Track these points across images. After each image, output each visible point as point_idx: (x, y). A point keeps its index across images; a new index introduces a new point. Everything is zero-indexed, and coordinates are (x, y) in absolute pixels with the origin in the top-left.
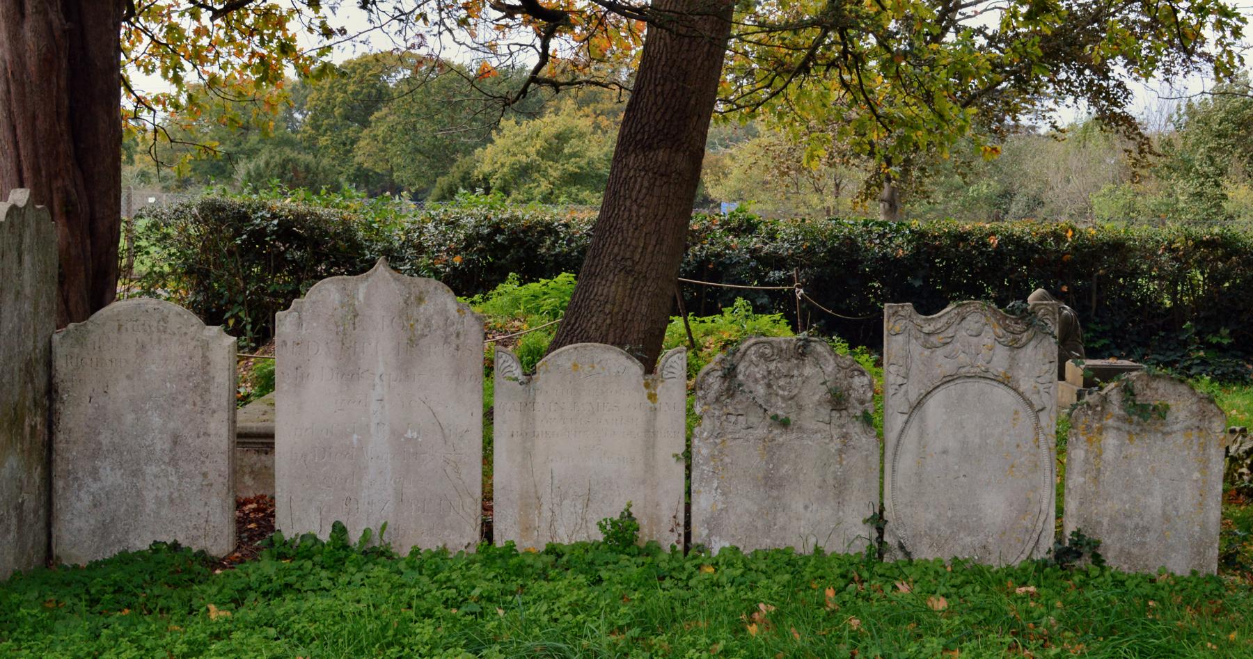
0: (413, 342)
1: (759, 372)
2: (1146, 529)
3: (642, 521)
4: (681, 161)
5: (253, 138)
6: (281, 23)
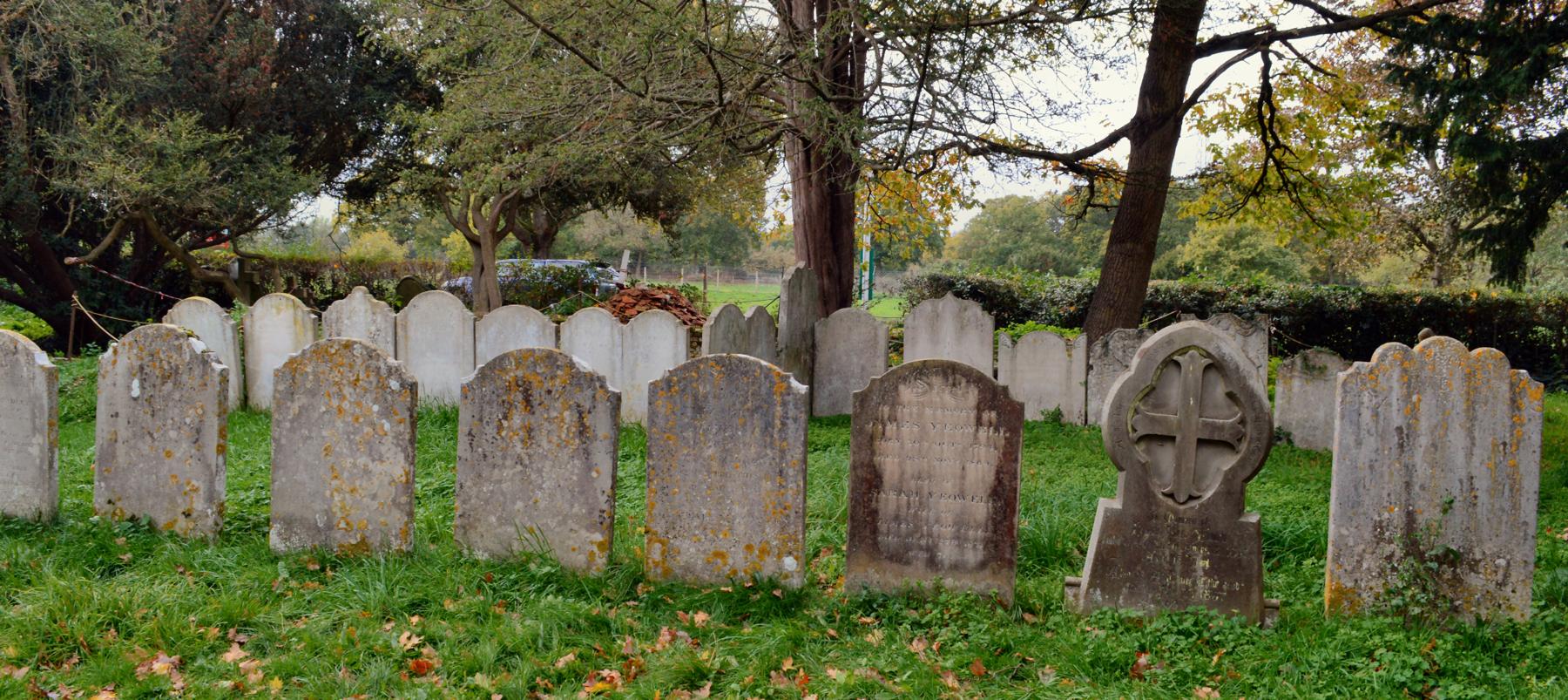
0: (962, 328)
1: (1120, 345)
2: (1315, 428)
3: (1065, 412)
4: (1140, 248)
5: (1027, 238)
6: (950, 180)
